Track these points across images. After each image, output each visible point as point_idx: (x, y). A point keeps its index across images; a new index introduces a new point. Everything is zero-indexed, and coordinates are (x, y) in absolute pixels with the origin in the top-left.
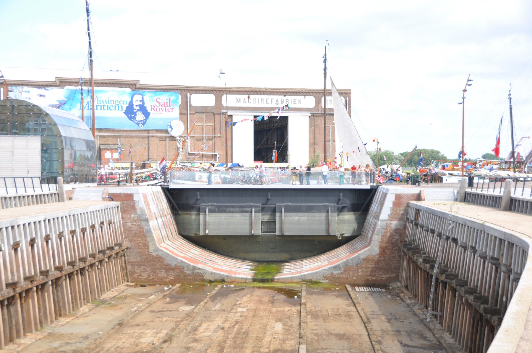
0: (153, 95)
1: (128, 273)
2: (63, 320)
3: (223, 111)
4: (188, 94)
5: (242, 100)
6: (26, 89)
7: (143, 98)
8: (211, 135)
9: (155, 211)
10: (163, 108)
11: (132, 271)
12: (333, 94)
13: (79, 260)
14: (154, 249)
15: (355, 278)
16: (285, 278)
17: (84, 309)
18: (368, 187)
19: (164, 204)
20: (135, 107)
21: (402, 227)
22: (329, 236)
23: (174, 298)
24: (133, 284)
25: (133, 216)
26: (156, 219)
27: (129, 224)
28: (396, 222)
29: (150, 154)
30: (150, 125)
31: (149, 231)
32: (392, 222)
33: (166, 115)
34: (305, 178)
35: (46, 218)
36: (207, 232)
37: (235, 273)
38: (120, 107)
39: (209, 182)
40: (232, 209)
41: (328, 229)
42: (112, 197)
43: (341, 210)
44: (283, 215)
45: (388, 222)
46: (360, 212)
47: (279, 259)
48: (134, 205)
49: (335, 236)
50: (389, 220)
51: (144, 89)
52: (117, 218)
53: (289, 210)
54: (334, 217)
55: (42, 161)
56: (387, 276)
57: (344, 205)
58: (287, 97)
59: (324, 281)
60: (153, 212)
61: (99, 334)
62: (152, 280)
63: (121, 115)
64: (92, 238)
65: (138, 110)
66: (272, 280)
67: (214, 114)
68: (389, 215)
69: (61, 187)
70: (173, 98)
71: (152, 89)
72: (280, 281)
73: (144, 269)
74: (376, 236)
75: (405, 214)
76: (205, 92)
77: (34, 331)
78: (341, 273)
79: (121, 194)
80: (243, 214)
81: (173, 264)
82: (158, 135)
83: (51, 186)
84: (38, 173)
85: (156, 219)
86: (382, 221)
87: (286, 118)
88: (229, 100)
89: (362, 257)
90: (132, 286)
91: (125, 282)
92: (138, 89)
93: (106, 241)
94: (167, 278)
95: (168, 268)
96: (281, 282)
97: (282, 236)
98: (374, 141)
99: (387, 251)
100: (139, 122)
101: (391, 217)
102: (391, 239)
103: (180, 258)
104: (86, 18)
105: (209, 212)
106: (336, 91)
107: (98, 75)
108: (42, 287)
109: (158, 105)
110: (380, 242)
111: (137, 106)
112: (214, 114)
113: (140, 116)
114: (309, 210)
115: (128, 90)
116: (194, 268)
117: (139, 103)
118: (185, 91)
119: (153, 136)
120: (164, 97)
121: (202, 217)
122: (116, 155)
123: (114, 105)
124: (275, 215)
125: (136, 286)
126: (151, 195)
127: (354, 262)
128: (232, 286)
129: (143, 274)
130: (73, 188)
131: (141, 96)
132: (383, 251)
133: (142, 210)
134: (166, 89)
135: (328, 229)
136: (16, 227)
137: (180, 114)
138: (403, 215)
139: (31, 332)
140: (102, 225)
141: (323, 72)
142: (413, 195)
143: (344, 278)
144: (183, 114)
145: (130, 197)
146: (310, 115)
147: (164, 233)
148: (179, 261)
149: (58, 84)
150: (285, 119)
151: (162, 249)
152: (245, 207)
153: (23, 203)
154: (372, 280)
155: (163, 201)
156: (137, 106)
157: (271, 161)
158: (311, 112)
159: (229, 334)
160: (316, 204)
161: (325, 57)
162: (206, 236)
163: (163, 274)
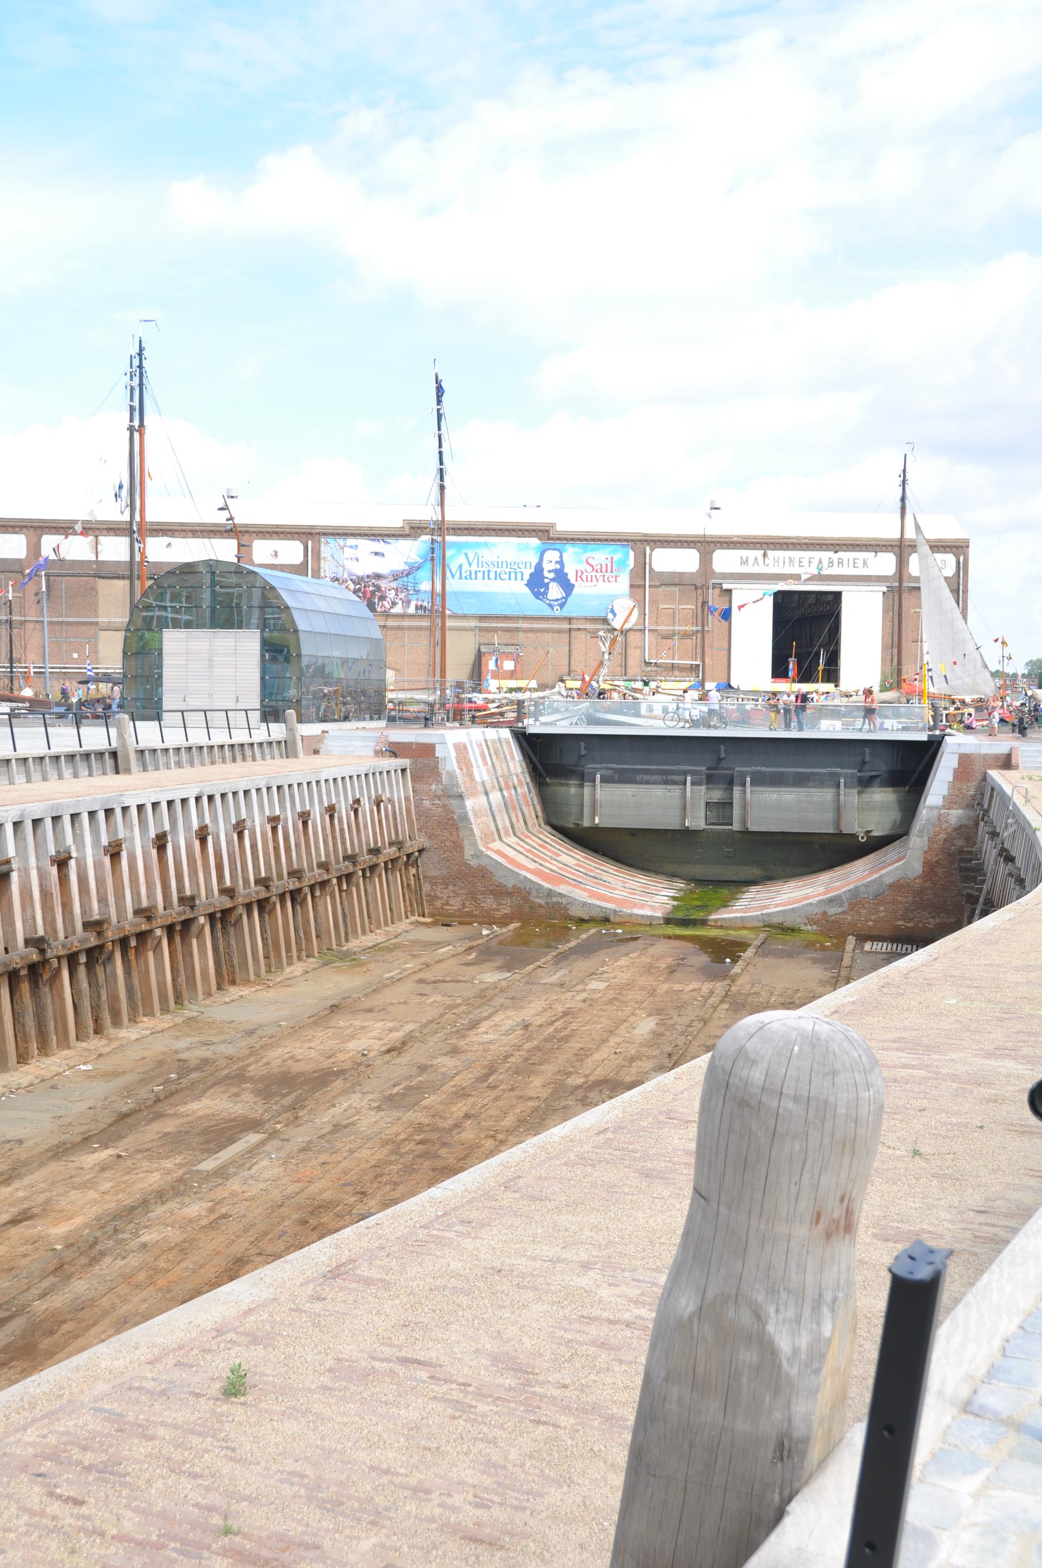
0: (581, 551)
1: (424, 898)
2: (234, 992)
3: (713, 581)
4: (648, 548)
5: (751, 561)
6: (351, 541)
7: (561, 557)
8: (692, 628)
9: (486, 777)
10: (598, 575)
11: (432, 894)
12: (919, 549)
13: (289, 874)
14: (472, 852)
15: (871, 923)
16: (730, 919)
17: (297, 968)
18: (923, 737)
19: (515, 763)
20: (546, 574)
21: (971, 823)
22: (841, 834)
23: (486, 954)
24: (429, 920)
25: (433, 787)
26: (487, 794)
27: (427, 803)
28: (960, 811)
29: (572, 663)
30: (572, 609)
31: (465, 818)
32: (950, 812)
33: (604, 590)
34: (794, 719)
35: (201, 792)
36: (597, 821)
37: (635, 905)
38: (519, 575)
39: (468, 734)
40: (646, 777)
41: (837, 822)
42: (395, 750)
43: (865, 783)
44: (748, 790)
45: (942, 811)
46: (907, 788)
47: (742, 877)
48: (437, 767)
49: (854, 836)
50: (944, 807)
51: (565, 539)
52: (399, 791)
53: (759, 780)
54: (851, 797)
55: (262, 679)
56: (938, 920)
57: (874, 773)
58: (841, 554)
59: (809, 928)
60: (478, 779)
61: (280, 1026)
62: (469, 914)
63: (520, 587)
64: (329, 832)
65: (552, 580)
66: (704, 923)
67: (696, 588)
68: (944, 797)
69: (291, 730)
70: (618, 557)
71: (579, 540)
72: (719, 924)
73: (454, 892)
74: (918, 839)
75: (979, 796)
76: (679, 544)
77: (158, 1013)
78: (844, 913)
79: (411, 743)
80: (669, 787)
81: (510, 884)
82: (589, 626)
83: (273, 726)
84: (253, 699)
85: (487, 794)
86: (931, 808)
87: (837, 596)
88: (724, 561)
89: (888, 881)
90: (426, 924)
91: (413, 914)
92: (553, 539)
93: (367, 837)
94: (498, 910)
95: (500, 892)
96: (722, 927)
97: (746, 833)
98: (996, 641)
99: (940, 871)
100: (553, 603)
101: (950, 802)
102: (947, 845)
103: (523, 873)
104: (436, 407)
105: (602, 781)
106: (924, 542)
107: (454, 514)
108: (180, 930)
109: (590, 569)
110: (926, 852)
111: (549, 572)
112: (696, 588)
113: (555, 592)
114: (800, 781)
115: (535, 542)
116: (550, 893)
117: (553, 566)
118: (642, 544)
119: (579, 629)
120: (600, 555)
121: (587, 790)
122: (509, 665)
123: (508, 570)
124: (732, 790)
125: (434, 924)
126: (480, 745)
127: (871, 890)
128: (620, 931)
129: (452, 901)
130: (323, 732)
131: (558, 554)
132: (930, 868)
133: (452, 776)
134: (606, 540)
135: (837, 822)
136: (118, 812)
137: (631, 586)
138: (973, 797)
139: (149, 1013)
140: (356, 806)
141: (899, 504)
142: (997, 757)
143: (849, 923)
144: (636, 587)
145: (427, 750)
146: (885, 589)
147: (503, 821)
148: (521, 878)
149: (407, 532)
150: (836, 597)
151: (489, 853)
152: (673, 772)
153: (196, 761)
154: (907, 927)
155: (513, 758)
156: (549, 572)
157: (817, 682)
158: (888, 584)
159: (529, 1039)
160: (815, 770)
161: (904, 476)
162: (596, 829)
163: (489, 902)
